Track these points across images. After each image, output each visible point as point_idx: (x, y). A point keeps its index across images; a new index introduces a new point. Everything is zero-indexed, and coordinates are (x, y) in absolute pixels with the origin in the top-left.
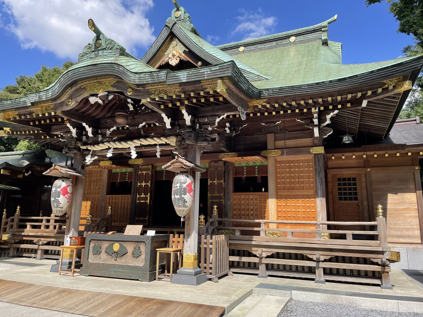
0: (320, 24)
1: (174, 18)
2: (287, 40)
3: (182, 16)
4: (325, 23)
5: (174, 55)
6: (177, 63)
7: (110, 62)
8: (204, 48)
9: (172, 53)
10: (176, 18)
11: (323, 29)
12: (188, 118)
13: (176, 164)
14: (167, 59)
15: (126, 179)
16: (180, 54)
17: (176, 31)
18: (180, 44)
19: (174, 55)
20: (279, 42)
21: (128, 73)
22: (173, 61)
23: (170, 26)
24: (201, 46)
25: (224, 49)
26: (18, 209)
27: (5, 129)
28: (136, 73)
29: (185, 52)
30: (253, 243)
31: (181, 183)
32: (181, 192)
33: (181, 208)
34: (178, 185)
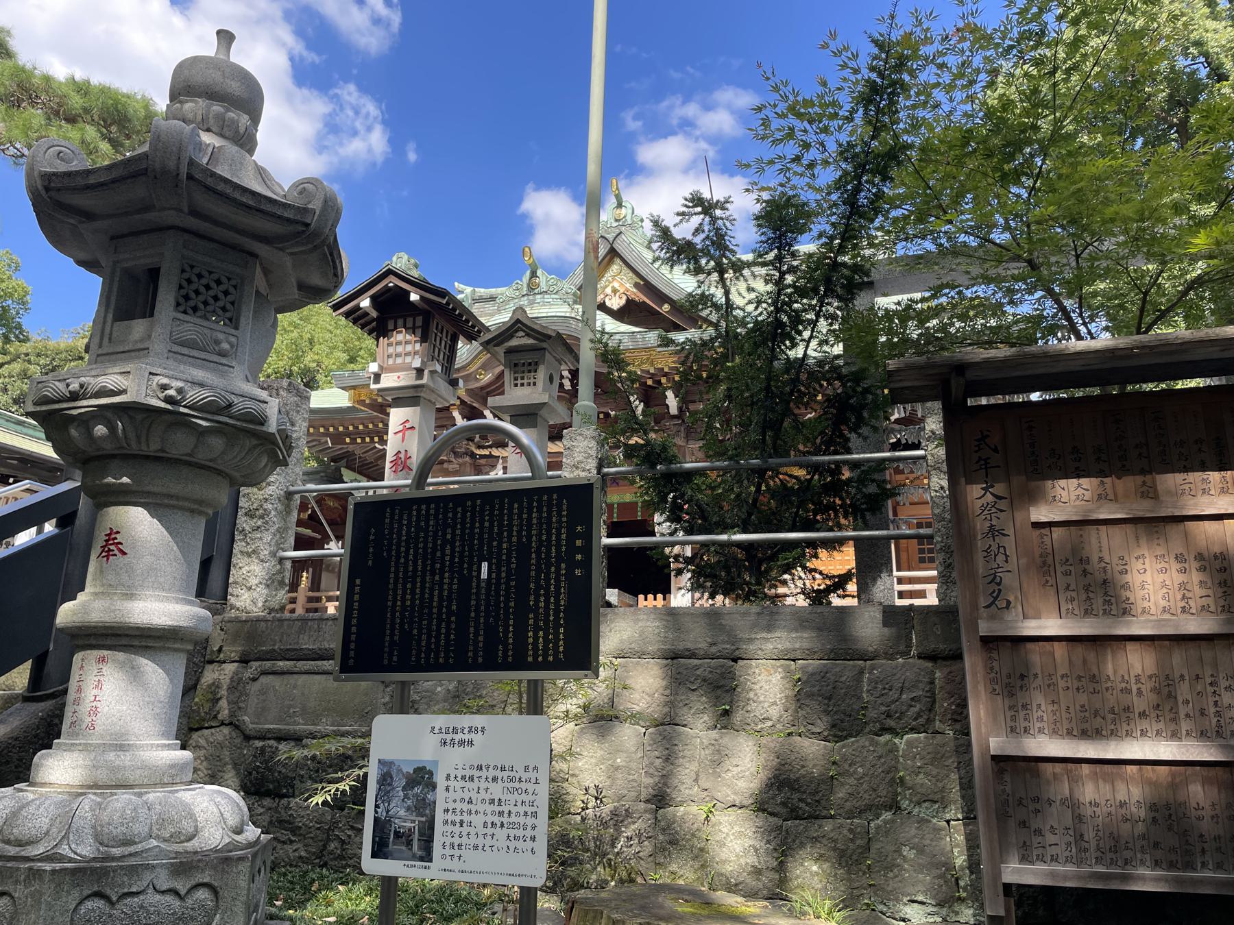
5: (615, 291)
7: (563, 314)
9: (613, 287)
12: (672, 401)
14: (602, 296)
17: (616, 246)
18: (625, 269)
19: (615, 291)
22: (613, 300)
23: (610, 237)
26: (304, 579)
29: (636, 285)
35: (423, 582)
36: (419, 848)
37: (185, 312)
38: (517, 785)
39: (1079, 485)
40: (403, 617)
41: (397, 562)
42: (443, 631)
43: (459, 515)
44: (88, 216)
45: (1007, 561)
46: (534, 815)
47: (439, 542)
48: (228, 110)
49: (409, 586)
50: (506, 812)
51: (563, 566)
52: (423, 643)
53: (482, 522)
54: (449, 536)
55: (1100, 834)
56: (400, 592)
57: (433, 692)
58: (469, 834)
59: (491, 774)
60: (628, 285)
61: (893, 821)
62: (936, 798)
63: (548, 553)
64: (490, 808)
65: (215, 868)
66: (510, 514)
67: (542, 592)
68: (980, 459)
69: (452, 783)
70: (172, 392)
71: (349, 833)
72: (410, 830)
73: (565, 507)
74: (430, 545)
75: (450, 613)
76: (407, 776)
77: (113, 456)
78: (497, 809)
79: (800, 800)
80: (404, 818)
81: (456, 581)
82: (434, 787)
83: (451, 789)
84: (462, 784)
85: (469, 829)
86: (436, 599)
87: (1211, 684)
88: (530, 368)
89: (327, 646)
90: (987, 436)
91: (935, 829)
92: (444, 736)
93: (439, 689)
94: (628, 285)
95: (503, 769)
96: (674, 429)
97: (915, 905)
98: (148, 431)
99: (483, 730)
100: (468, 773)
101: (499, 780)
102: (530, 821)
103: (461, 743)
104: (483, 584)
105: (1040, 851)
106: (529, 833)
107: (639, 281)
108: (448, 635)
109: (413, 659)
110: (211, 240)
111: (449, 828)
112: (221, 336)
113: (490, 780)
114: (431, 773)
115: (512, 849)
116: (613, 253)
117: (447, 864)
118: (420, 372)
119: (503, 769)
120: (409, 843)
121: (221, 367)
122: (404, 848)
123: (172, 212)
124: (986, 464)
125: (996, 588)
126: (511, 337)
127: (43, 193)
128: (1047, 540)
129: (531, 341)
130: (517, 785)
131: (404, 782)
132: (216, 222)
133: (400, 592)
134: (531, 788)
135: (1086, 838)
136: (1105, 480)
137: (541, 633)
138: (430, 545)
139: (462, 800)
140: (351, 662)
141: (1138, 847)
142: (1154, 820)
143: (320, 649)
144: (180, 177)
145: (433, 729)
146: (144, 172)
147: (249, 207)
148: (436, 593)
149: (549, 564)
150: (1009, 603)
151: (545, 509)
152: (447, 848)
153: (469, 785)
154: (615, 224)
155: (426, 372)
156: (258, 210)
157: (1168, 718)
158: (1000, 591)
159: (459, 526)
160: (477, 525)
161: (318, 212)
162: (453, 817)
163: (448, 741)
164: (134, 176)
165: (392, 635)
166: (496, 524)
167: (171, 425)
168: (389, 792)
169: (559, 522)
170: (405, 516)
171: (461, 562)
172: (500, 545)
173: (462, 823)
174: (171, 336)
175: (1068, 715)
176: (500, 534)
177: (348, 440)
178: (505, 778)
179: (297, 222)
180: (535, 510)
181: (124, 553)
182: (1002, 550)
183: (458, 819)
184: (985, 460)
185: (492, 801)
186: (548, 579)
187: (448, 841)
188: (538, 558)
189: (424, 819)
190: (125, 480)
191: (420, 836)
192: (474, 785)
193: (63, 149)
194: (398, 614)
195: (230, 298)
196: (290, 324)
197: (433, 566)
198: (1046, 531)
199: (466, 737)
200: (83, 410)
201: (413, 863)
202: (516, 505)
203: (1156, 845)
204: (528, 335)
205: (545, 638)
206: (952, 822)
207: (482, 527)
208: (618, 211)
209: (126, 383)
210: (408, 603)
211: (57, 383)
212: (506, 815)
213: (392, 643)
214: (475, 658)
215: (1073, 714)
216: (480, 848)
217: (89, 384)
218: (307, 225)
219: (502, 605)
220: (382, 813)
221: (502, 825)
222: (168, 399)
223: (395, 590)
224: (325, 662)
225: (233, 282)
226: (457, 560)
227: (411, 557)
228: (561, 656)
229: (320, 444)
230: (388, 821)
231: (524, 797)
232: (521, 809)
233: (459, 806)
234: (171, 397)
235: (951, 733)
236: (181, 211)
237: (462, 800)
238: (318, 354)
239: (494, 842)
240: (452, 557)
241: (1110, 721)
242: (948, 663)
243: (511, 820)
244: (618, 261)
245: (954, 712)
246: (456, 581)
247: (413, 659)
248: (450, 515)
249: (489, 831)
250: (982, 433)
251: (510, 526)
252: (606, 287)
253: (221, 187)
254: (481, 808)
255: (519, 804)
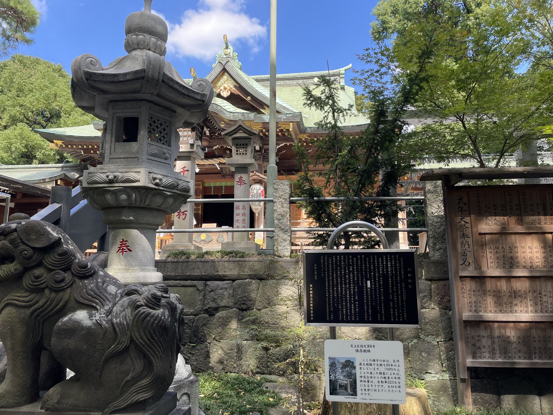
0: (339, 69)
1: (224, 55)
2: (311, 80)
3: (231, 54)
4: (342, 70)
6: (228, 95)
8: (254, 86)
10: (225, 55)
11: (341, 76)
13: (254, 177)
15: (222, 192)
16: (231, 88)
17: (226, 67)
18: (230, 79)
19: (225, 88)
20: (305, 80)
21: (225, 112)
23: (224, 63)
24: (251, 84)
25: (257, 80)
27: (55, 141)
28: (231, 112)
29: (235, 86)
30: (297, 236)
31: (257, 190)
32: (257, 196)
33: (257, 207)
34: (255, 191)
35: (341, 287)
36: (351, 391)
37: (163, 144)
38: (391, 367)
39: (495, 219)
40: (334, 301)
41: (329, 278)
42: (353, 307)
43: (355, 261)
44: (104, 92)
45: (469, 247)
46: (399, 378)
47: (347, 272)
48: (158, 40)
49: (335, 288)
50: (387, 377)
51: (403, 284)
52: (344, 312)
53: (366, 264)
54: (351, 269)
55: (501, 348)
56: (331, 291)
57: (223, 295)
58: (372, 385)
59: (379, 363)
60: (231, 86)
61: (418, 343)
62: (434, 333)
63: (396, 278)
64: (380, 376)
65: (188, 386)
66: (378, 262)
67: (395, 294)
68: (459, 207)
69: (362, 366)
70: (157, 181)
71: (189, 355)
72: (346, 384)
73: (402, 260)
74: (343, 272)
75: (355, 301)
76: (342, 363)
77: (124, 207)
78: (383, 376)
79: (382, 336)
80: (342, 379)
81: (356, 288)
82: (355, 368)
83: (362, 369)
84: (367, 367)
85: (372, 384)
86: (348, 294)
87: (539, 294)
88: (243, 146)
89: (170, 274)
90: (462, 198)
91: (434, 345)
92: (357, 348)
93: (225, 293)
94: (231, 86)
95: (384, 361)
96: (258, 157)
97: (428, 374)
98: (146, 197)
99: (374, 346)
100: (369, 362)
101: (383, 365)
102: (397, 380)
103: (365, 351)
104: (369, 290)
105: (480, 355)
106: (397, 385)
107: (236, 85)
108: (355, 309)
109: (340, 318)
110: (159, 105)
111: (363, 383)
112: (166, 151)
113: (379, 365)
114: (353, 363)
115: (391, 391)
116: (224, 70)
117: (364, 396)
118: (192, 145)
119: (384, 361)
120: (346, 389)
121: (166, 165)
122: (344, 391)
123: (149, 95)
124: (462, 209)
125: (465, 257)
126: (237, 132)
127: (85, 81)
128: (483, 239)
129: (246, 135)
130: (391, 367)
131: (341, 366)
132: (166, 99)
133: (331, 291)
134: (397, 368)
135: (496, 350)
136: (505, 217)
137: (396, 310)
138: (343, 272)
139: (368, 373)
140: (312, 318)
141: (513, 352)
142: (519, 342)
143: (166, 276)
144: (159, 81)
145: (352, 346)
146: (143, 78)
147: (184, 94)
148: (348, 292)
149: (397, 283)
150: (469, 263)
151: (393, 261)
152: (363, 391)
153: (370, 367)
154: (225, 56)
155: (195, 145)
156: (188, 96)
157: (524, 306)
158: (466, 258)
159: (355, 265)
160: (364, 265)
161: (208, 95)
162: (364, 379)
163: (359, 350)
164: (137, 79)
165: (330, 308)
166: (372, 266)
167: (154, 195)
168: (335, 370)
169: (400, 266)
170: (330, 260)
171: (358, 280)
172: (375, 275)
173: (368, 381)
174: (148, 152)
175: (490, 305)
176: (374, 269)
177: (92, 152)
178: (385, 365)
179: (200, 100)
180: (389, 261)
181: (130, 251)
182: (467, 243)
183: (366, 380)
184: (461, 208)
185: (381, 373)
186: (397, 289)
187: (363, 388)
188: (392, 280)
189: (351, 380)
190: (131, 218)
191: (351, 386)
192: (373, 367)
193: (93, 59)
194: (331, 300)
195: (166, 132)
196: (44, 86)
197: (345, 281)
198: (483, 236)
199: (367, 349)
200: (116, 188)
201: (349, 397)
202: (380, 259)
203: (520, 351)
204: (244, 132)
205: (398, 311)
206: (439, 343)
207: (366, 266)
208: (226, 50)
209: (138, 177)
210: (336, 295)
211: (100, 174)
212: (387, 378)
213: (330, 311)
214: (368, 318)
215: (492, 305)
216: (377, 391)
217: (119, 176)
218: (203, 101)
219: (378, 298)
220: (333, 378)
221: (386, 382)
222: (157, 184)
223: (329, 290)
224: (169, 281)
225: (167, 125)
226: (356, 279)
227: (335, 277)
228: (406, 319)
229: (77, 152)
230: (336, 381)
231: (394, 371)
232: (394, 376)
233: (366, 375)
234: (158, 183)
235: (438, 309)
236: (153, 94)
237: (368, 373)
238: (59, 102)
239: (383, 388)
240: (354, 278)
241: (504, 307)
242: (437, 282)
243: (389, 380)
244: (226, 74)
245: (439, 301)
246: (356, 288)
247: (340, 318)
248: (351, 261)
249: (381, 384)
250: (460, 197)
251: (378, 267)
252: (221, 86)
253: (176, 86)
254: (376, 375)
255: (392, 374)
